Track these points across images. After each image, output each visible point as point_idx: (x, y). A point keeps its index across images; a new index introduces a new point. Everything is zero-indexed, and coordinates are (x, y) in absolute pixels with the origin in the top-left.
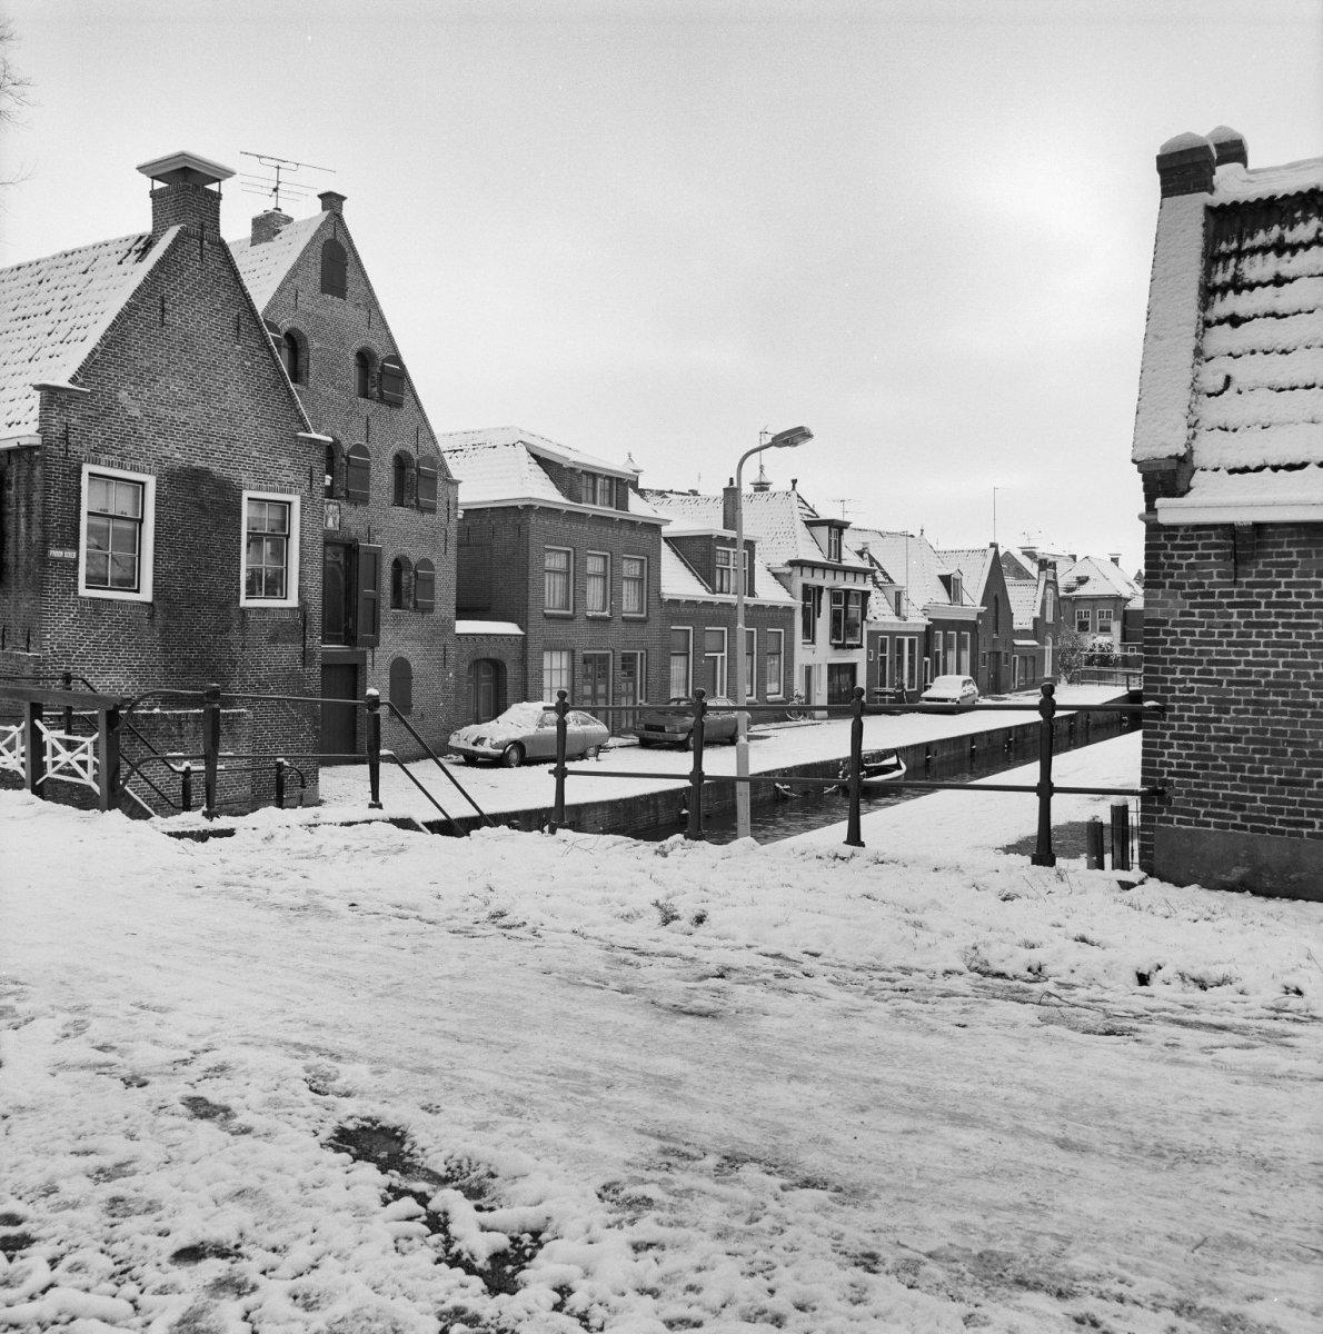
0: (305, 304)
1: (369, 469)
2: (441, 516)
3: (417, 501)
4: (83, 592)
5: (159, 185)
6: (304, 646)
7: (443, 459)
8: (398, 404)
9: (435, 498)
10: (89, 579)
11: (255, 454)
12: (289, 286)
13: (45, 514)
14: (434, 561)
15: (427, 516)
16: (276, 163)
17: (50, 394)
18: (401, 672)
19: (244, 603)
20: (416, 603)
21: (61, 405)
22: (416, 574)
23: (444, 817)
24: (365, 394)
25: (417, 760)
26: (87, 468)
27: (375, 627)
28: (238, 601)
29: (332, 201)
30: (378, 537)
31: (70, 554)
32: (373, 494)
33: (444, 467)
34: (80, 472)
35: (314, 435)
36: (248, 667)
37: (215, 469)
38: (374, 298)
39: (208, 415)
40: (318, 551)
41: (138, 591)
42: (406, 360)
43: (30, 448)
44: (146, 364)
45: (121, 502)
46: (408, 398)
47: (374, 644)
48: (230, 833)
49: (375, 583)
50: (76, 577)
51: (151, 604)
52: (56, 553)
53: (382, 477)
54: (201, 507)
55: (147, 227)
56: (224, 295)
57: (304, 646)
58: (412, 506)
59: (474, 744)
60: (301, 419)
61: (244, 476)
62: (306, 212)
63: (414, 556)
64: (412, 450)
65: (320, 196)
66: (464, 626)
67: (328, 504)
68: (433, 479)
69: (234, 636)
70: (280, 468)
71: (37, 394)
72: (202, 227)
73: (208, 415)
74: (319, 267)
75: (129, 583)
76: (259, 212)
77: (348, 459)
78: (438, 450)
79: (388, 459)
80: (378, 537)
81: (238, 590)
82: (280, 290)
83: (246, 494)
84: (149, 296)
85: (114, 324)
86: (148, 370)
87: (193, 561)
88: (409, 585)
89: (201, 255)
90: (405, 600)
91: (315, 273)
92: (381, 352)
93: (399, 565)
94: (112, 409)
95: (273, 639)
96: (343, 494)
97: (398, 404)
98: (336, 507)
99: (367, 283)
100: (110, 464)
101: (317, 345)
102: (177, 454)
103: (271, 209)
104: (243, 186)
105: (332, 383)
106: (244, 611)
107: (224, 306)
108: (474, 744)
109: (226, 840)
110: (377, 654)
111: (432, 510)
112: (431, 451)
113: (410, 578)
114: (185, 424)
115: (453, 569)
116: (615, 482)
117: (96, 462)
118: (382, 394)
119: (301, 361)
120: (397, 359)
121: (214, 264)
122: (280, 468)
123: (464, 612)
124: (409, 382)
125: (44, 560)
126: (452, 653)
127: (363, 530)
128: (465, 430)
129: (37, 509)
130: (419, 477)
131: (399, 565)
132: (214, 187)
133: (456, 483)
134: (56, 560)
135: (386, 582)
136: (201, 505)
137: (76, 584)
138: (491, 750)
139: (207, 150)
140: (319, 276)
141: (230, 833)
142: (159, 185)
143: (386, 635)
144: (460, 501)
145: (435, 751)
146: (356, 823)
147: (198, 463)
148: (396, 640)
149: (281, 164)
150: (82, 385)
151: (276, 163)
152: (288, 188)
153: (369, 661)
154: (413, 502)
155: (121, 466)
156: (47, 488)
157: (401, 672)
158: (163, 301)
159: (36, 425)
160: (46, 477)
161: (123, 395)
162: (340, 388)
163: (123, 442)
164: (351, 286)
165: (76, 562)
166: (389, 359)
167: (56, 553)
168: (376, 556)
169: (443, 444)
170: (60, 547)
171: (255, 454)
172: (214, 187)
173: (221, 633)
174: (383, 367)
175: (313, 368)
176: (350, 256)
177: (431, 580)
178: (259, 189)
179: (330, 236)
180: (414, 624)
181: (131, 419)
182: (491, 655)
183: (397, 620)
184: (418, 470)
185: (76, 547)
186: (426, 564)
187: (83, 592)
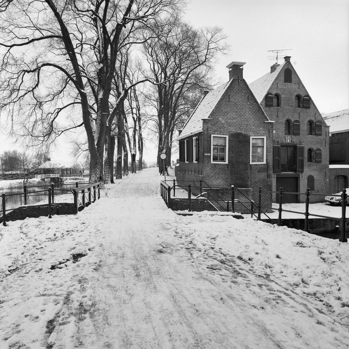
0: (280, 86)
1: (300, 126)
2: (323, 137)
3: (315, 133)
4: (212, 162)
5: (231, 69)
6: (268, 173)
7: (324, 121)
8: (309, 108)
9: (321, 131)
10: (213, 159)
11: (253, 128)
12: (275, 83)
13: (204, 146)
14: (321, 149)
15: (319, 137)
16: (276, 52)
17: (204, 121)
18: (311, 179)
19: (251, 163)
20: (315, 161)
21: (207, 123)
22: (315, 153)
23: (268, 218)
24: (299, 106)
25: (316, 203)
26: (212, 136)
27: (302, 167)
28: (249, 163)
29: (287, 59)
30: (303, 144)
31: (209, 154)
32: (301, 132)
33: (324, 123)
34: (211, 136)
35: (270, 121)
36: (252, 178)
37: (243, 132)
38: (300, 81)
39: (241, 120)
40: (272, 150)
41: (225, 162)
42: (311, 95)
43: (202, 132)
44: (226, 111)
45: (220, 142)
46: (312, 105)
47: (302, 172)
48: (192, 215)
49: (302, 155)
50: (210, 159)
51: (228, 164)
52: (206, 154)
53: (304, 127)
54: (239, 141)
55: (229, 80)
56: (244, 92)
57: (268, 173)
58: (314, 135)
59: (331, 199)
60: (266, 118)
61: (251, 133)
62: (282, 62)
63: (315, 148)
64: (313, 119)
65: (284, 58)
66: (332, 166)
67: (288, 136)
68: (321, 126)
69: (249, 171)
70: (260, 130)
71: (202, 121)
72: (238, 77)
73: (241, 120)
74: (284, 76)
75: (223, 159)
76: (272, 65)
77: (293, 124)
78: (322, 118)
79: (306, 122)
80: (303, 144)
81: (250, 160)
82: (273, 84)
83: (251, 138)
84: (226, 96)
85: (218, 103)
86: (226, 112)
87: (238, 154)
88: (313, 156)
89: (238, 84)
90: (312, 160)
91: (282, 78)
92: (302, 94)
93: (310, 150)
94: (218, 121)
95: (259, 172)
96: (292, 133)
97: (309, 108)
98: (290, 137)
99: (298, 77)
100: (218, 134)
101: (283, 96)
102: (233, 130)
103: (275, 64)
104: (268, 57)
105: (288, 105)
106: (251, 165)
107: (244, 94)
108: (331, 199)
109: (190, 216)
110: (303, 174)
111: (321, 135)
112: (320, 119)
113: (314, 154)
114: (235, 123)
115: (328, 151)
116: (223, 147)
117: (214, 134)
118: (303, 106)
119: (280, 101)
120: (308, 96)
121: (242, 85)
122: (260, 130)
123: (332, 162)
124: (312, 101)
125: (204, 156)
126: (328, 174)
127: (298, 142)
128: (343, 109)
129: (203, 145)
130: (317, 126)
131: (310, 150)
132: (241, 67)
133: (329, 127)
134: (206, 156)
135: (306, 155)
136: (240, 142)
137: (210, 161)
138: (335, 201)
139: (238, 60)
140: (284, 78)
141: (192, 215)
142: (231, 69)
143: (306, 169)
144: (330, 132)
145: (323, 201)
146: (229, 215)
147: (239, 132)
148: (309, 170)
149: (278, 51)
150: (211, 118)
151: (276, 52)
152: (274, 59)
153: (301, 176)
154: (314, 133)
155: (220, 134)
156: (204, 140)
157: (311, 179)
158: (229, 96)
159: (202, 128)
160: (204, 138)
161: (220, 119)
162: (291, 106)
163: (220, 129)
164: (293, 79)
165: (210, 156)
166: (305, 96)
167: (206, 154)
168: (302, 149)
169: (323, 116)
170: (207, 153)
171: (253, 128)
172: (241, 67)
173: (245, 170)
174: (303, 99)
175: (282, 102)
176: (293, 72)
177: (321, 154)
178: (273, 59)
179: (287, 68)
180: (315, 166)
181: (222, 124)
182: (343, 174)
183: (309, 165)
184: (315, 124)
185: (210, 153)
186: (319, 150)
187: (212, 162)
